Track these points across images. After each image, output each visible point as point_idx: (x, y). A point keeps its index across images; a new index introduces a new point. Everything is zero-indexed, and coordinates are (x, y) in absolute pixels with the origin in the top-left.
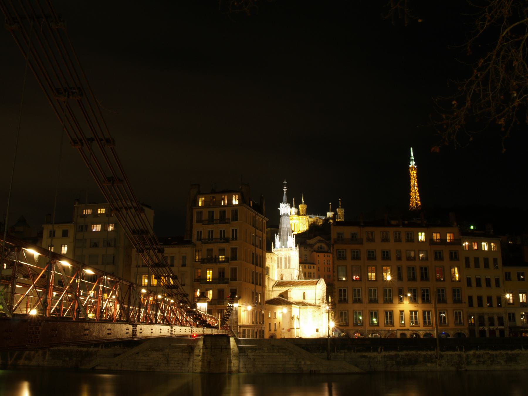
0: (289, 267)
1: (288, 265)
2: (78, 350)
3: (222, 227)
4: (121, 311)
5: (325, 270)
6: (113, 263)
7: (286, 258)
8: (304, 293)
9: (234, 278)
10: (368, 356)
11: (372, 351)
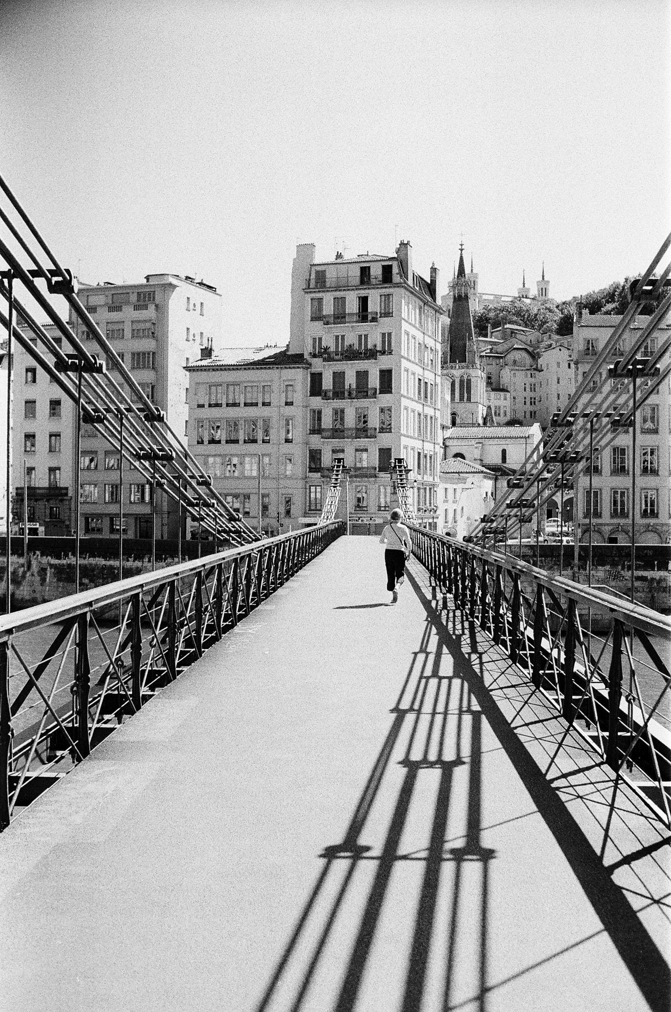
0: (469, 399)
1: (466, 395)
2: (105, 565)
3: (364, 328)
4: (463, 855)
5: (525, 402)
6: (287, 404)
7: (462, 382)
8: (504, 452)
9: (386, 428)
10: (649, 577)
11: (656, 569)
